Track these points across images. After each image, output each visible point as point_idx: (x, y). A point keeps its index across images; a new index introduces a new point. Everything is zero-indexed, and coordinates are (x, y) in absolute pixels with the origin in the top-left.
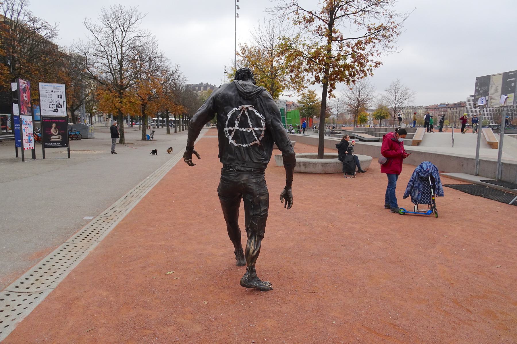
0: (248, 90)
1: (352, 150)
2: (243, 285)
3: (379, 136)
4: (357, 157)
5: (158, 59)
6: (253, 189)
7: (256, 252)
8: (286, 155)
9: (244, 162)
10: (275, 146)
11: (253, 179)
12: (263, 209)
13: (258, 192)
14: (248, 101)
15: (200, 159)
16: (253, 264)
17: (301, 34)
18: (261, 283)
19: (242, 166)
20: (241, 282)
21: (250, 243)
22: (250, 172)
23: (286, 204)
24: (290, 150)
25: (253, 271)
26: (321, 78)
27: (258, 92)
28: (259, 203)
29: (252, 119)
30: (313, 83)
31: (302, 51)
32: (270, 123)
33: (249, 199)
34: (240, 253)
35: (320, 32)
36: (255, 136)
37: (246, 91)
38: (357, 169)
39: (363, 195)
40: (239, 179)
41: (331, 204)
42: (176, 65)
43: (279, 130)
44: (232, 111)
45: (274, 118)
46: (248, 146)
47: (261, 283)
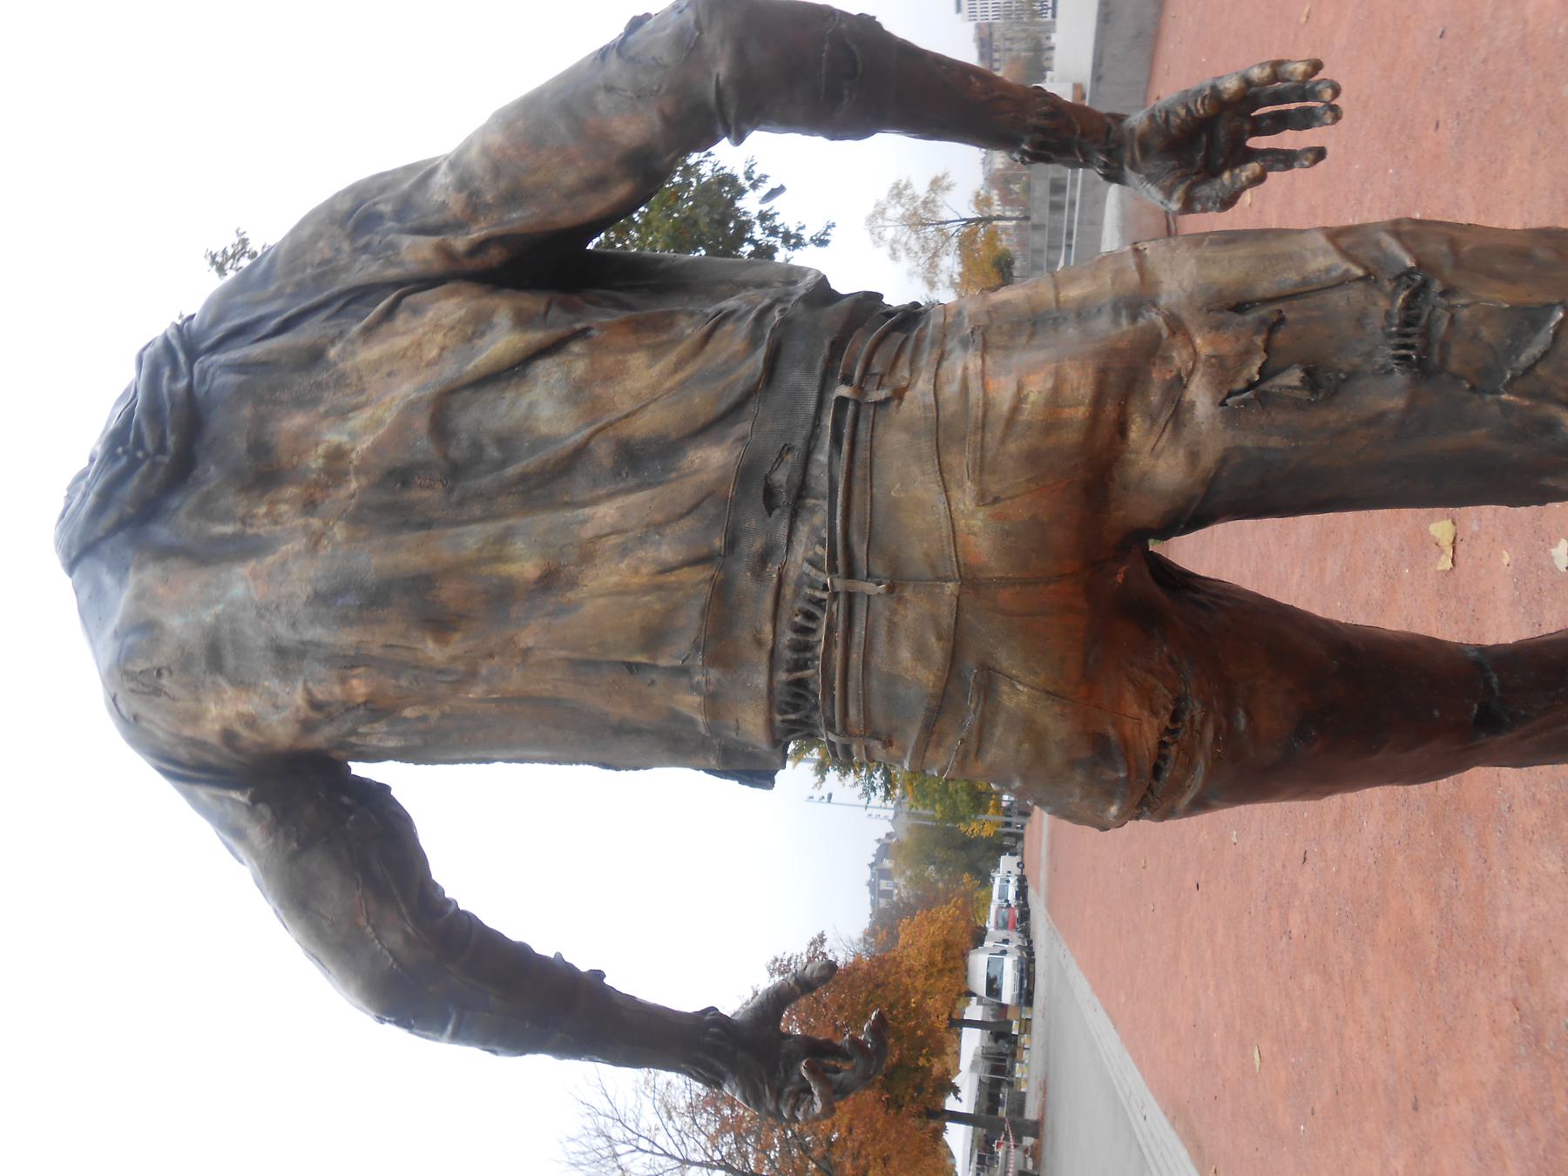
23: (1286, 159)
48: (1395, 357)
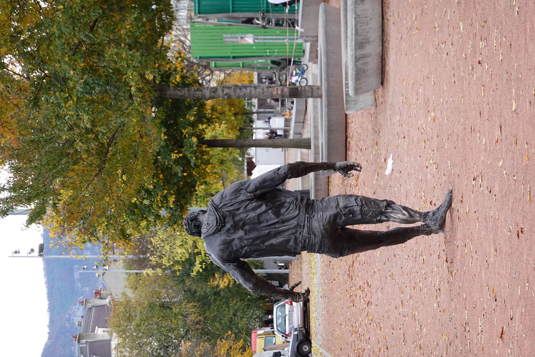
8: (290, 176)
9: (298, 225)
14: (226, 221)
15: (301, 282)
22: (310, 219)
32: (252, 195)
37: (215, 224)
43: (259, 184)
45: (246, 189)
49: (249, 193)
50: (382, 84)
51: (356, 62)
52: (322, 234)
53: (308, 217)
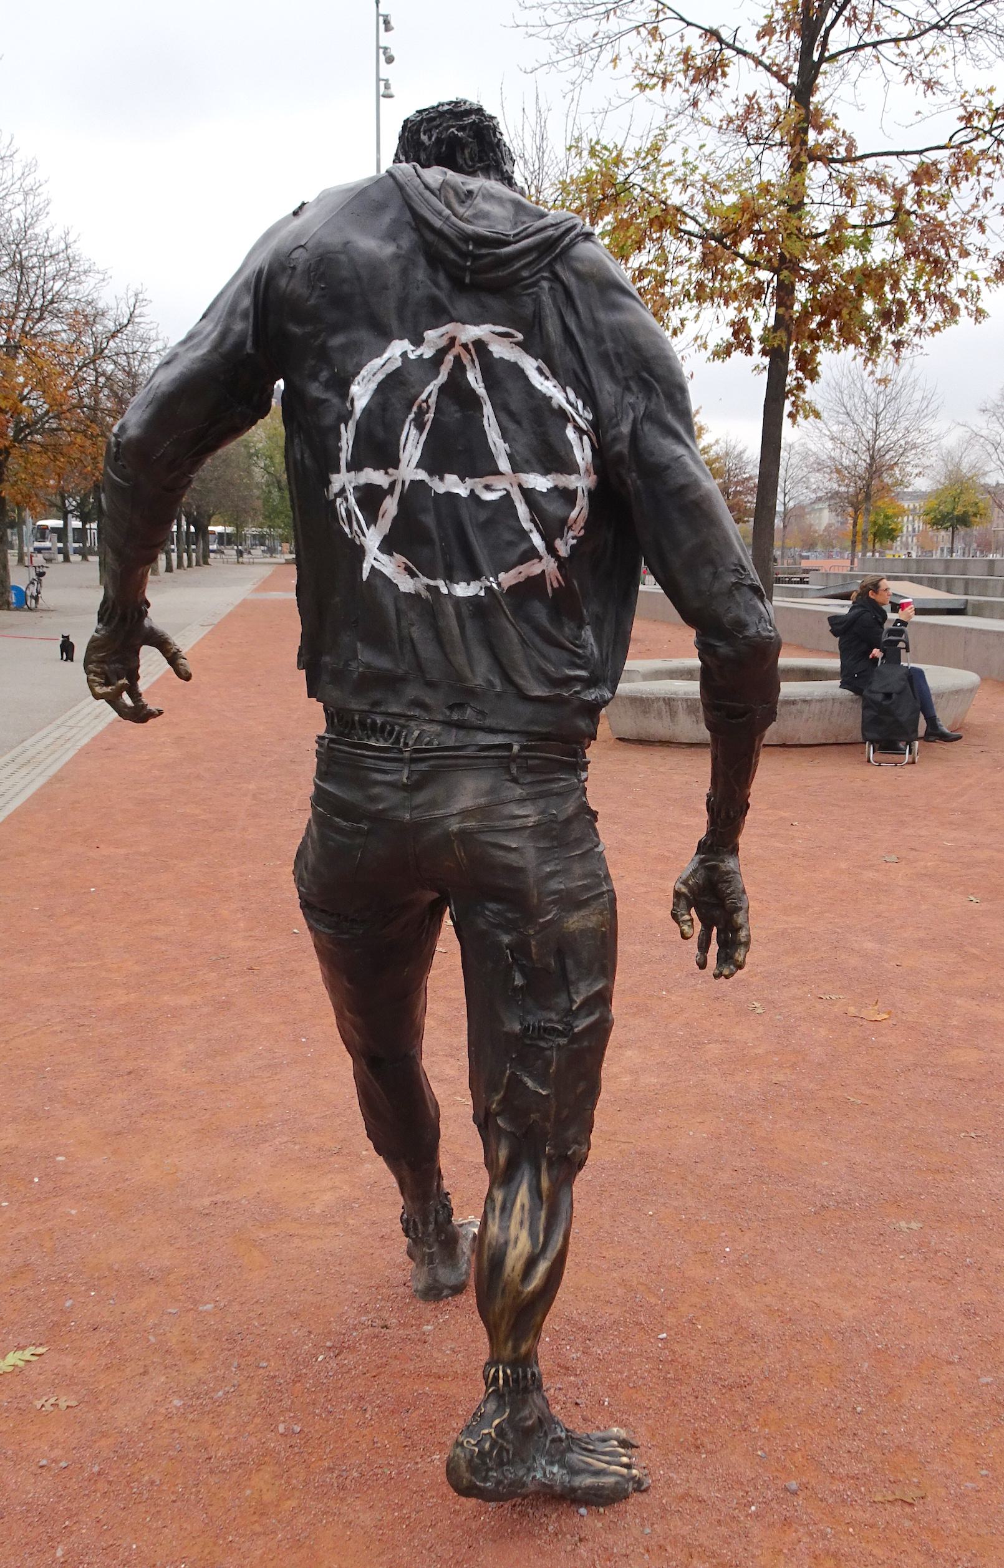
0: (485, 222)
1: (901, 645)
2: (467, 1491)
3: (962, 590)
4: (920, 673)
5: (51, 269)
6: (521, 870)
7: (543, 1267)
8: (723, 649)
10: (649, 586)
11: (521, 801)
12: (582, 993)
13: (555, 885)
15: (187, 677)
16: (524, 1349)
17: (670, 133)
18: (576, 1458)
19: (448, 724)
20: (451, 1470)
21: (503, 1209)
23: (704, 946)
24: (751, 619)
25: (526, 1390)
26: (756, 331)
27: (549, 245)
28: (560, 954)
29: (512, 415)
30: (725, 352)
31: (678, 204)
32: (622, 447)
33: (498, 932)
34: (431, 1227)
35: (752, 129)
36: (527, 525)
37: (469, 228)
38: (922, 726)
39: (976, 846)
40: (433, 804)
41: (843, 892)
42: (131, 293)
43: (683, 488)
44: (378, 362)
45: (652, 417)
46: (489, 589)
47: (576, 1458)
48: (529, 1025)
49: (634, 433)
50: (620, 739)
51: (664, 699)
52: (418, 827)
53: (509, 747)
